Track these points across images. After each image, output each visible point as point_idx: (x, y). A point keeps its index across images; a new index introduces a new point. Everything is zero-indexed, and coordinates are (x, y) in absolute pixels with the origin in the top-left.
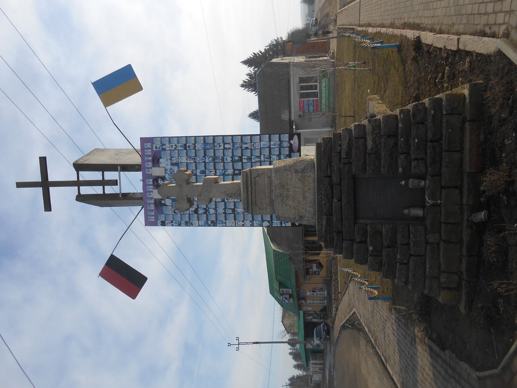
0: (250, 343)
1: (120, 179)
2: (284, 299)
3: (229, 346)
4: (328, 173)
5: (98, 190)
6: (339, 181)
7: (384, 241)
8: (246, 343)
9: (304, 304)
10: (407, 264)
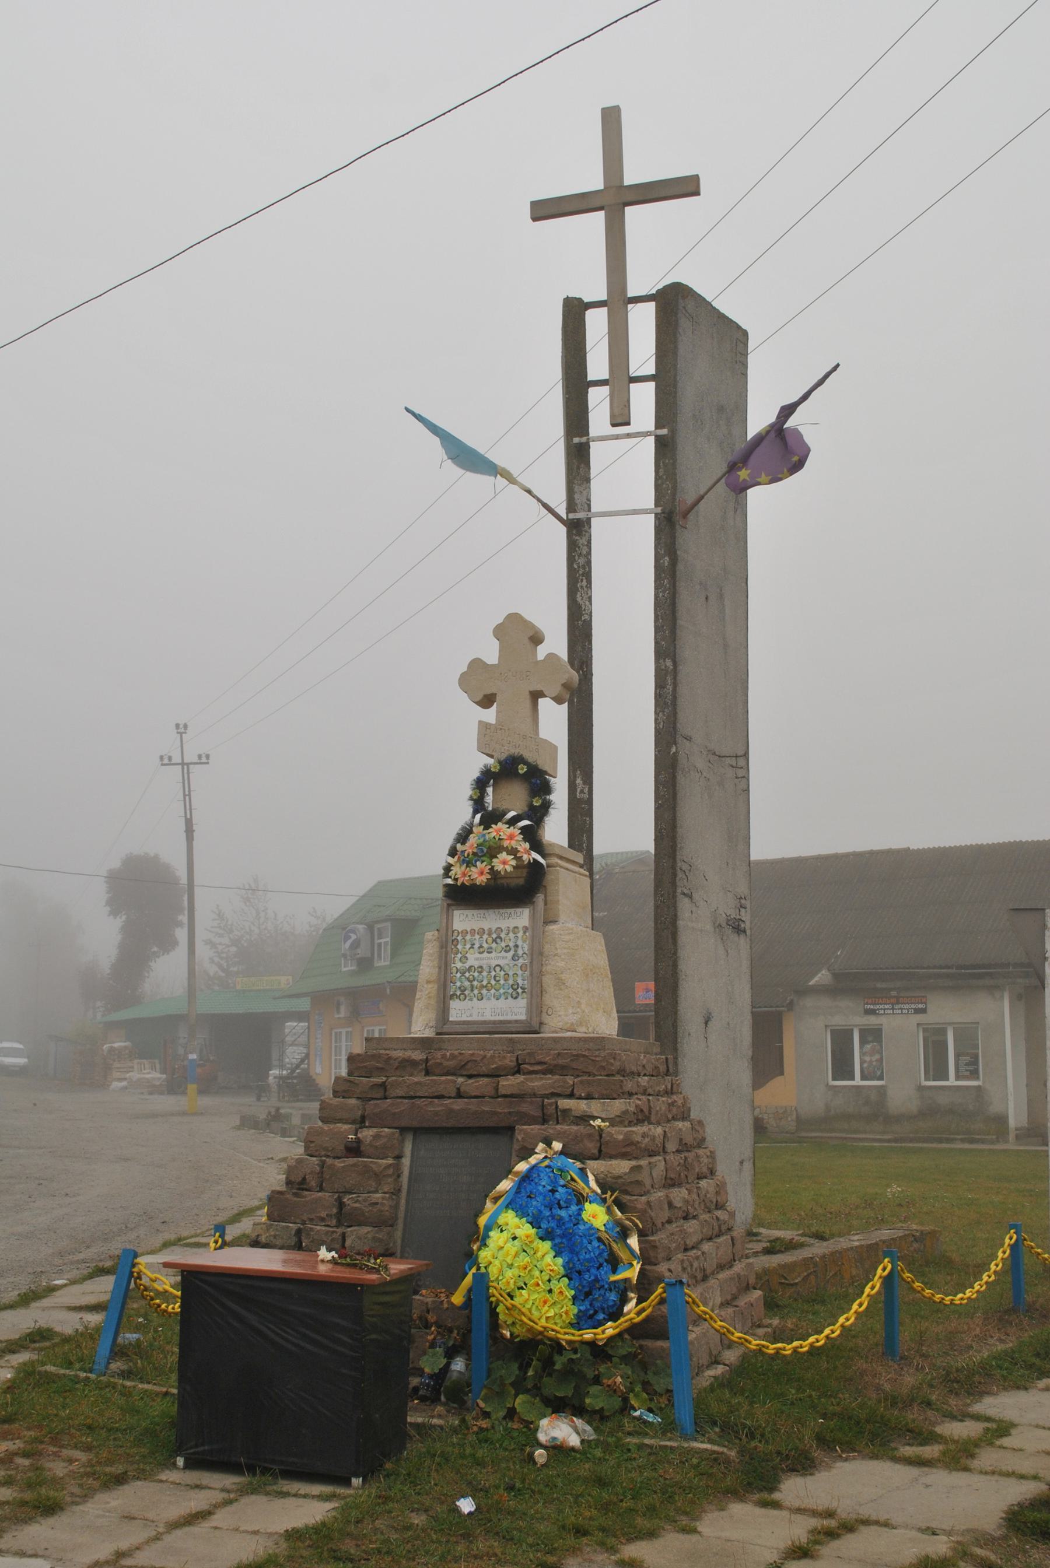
0: (188, 807)
1: (628, 436)
2: (354, 937)
3: (177, 726)
5: (597, 366)
8: (189, 791)
9: (337, 1016)
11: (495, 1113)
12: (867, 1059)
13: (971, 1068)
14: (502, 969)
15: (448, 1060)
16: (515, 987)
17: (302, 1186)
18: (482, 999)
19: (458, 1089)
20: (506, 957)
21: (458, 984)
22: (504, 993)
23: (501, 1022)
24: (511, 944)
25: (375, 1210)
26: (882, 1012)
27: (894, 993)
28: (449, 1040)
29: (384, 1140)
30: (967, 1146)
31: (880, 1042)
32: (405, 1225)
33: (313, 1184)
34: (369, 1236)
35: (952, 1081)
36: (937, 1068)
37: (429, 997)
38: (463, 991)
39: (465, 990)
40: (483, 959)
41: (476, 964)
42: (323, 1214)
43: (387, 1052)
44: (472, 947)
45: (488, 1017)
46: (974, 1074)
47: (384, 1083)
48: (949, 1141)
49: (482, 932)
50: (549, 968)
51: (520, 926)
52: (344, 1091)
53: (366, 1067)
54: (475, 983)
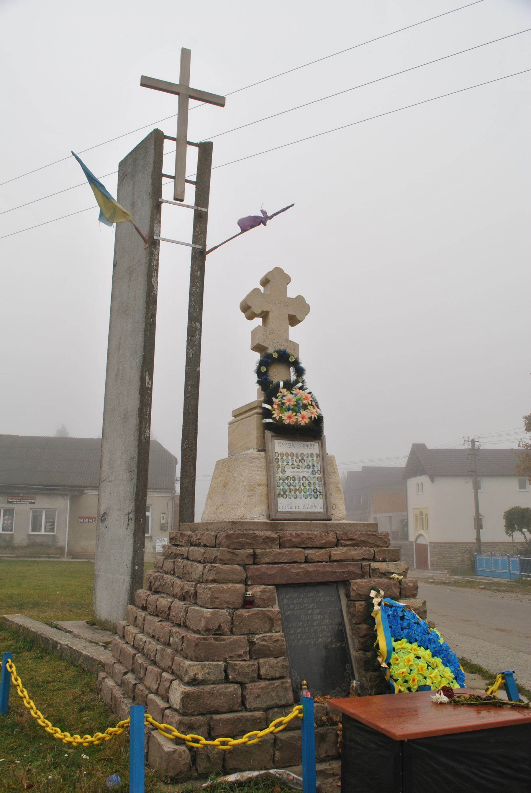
1: (182, 205)
4: (343, 541)
6: (335, 559)
7: (261, 636)
10: (226, 680)
11: (335, 572)
12: (6, 522)
13: (51, 527)
14: (306, 479)
15: (295, 537)
16: (315, 491)
17: (217, 632)
18: (297, 497)
19: (306, 557)
20: (308, 472)
21: (281, 487)
22: (309, 495)
23: (310, 513)
24: (311, 464)
26: (15, 502)
27: (22, 495)
28: (288, 524)
29: (268, 594)
30: (47, 559)
31: (12, 515)
33: (227, 629)
34: (279, 665)
35: (43, 532)
36: (36, 526)
37: (262, 495)
38: (285, 492)
39: (286, 491)
40: (295, 472)
41: (291, 475)
42: (241, 652)
44: (287, 464)
45: (302, 509)
46: (52, 530)
48: (39, 557)
49: (292, 455)
50: (332, 480)
51: (315, 453)
52: (229, 560)
53: (240, 542)
54: (292, 487)
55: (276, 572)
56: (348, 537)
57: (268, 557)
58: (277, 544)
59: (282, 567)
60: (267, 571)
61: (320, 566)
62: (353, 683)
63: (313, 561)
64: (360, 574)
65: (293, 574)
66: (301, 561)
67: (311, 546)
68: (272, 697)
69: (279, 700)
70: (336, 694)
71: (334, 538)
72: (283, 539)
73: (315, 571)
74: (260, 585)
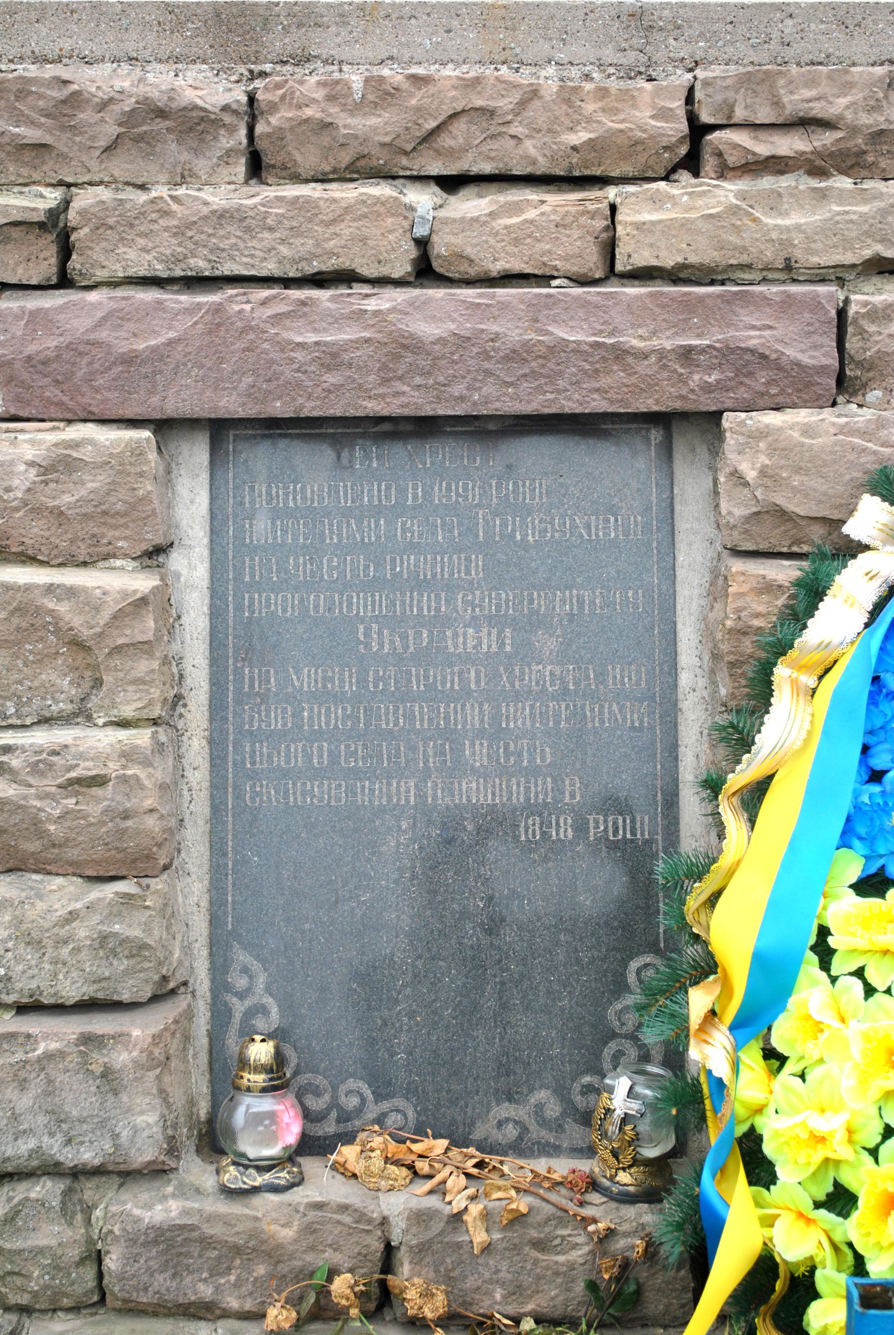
6: (644, 258)
11: (620, 354)
15: (357, 108)
19: (422, 244)
25: (94, 810)
29: (94, 483)
32: (217, 848)
34: (82, 932)
43: (59, 71)
47: (56, 214)
55: (170, 343)
56: (777, 104)
57: (141, 242)
58: (229, 153)
59: (218, 309)
60: (103, 335)
61: (504, 306)
62: (611, 1090)
63: (472, 272)
64: (822, 370)
65: (299, 355)
66: (384, 271)
67: (487, 168)
68: (15, 1117)
69: (60, 1138)
70: (525, 1129)
71: (663, 114)
72: (274, 120)
73: (463, 341)
74: (70, 422)
